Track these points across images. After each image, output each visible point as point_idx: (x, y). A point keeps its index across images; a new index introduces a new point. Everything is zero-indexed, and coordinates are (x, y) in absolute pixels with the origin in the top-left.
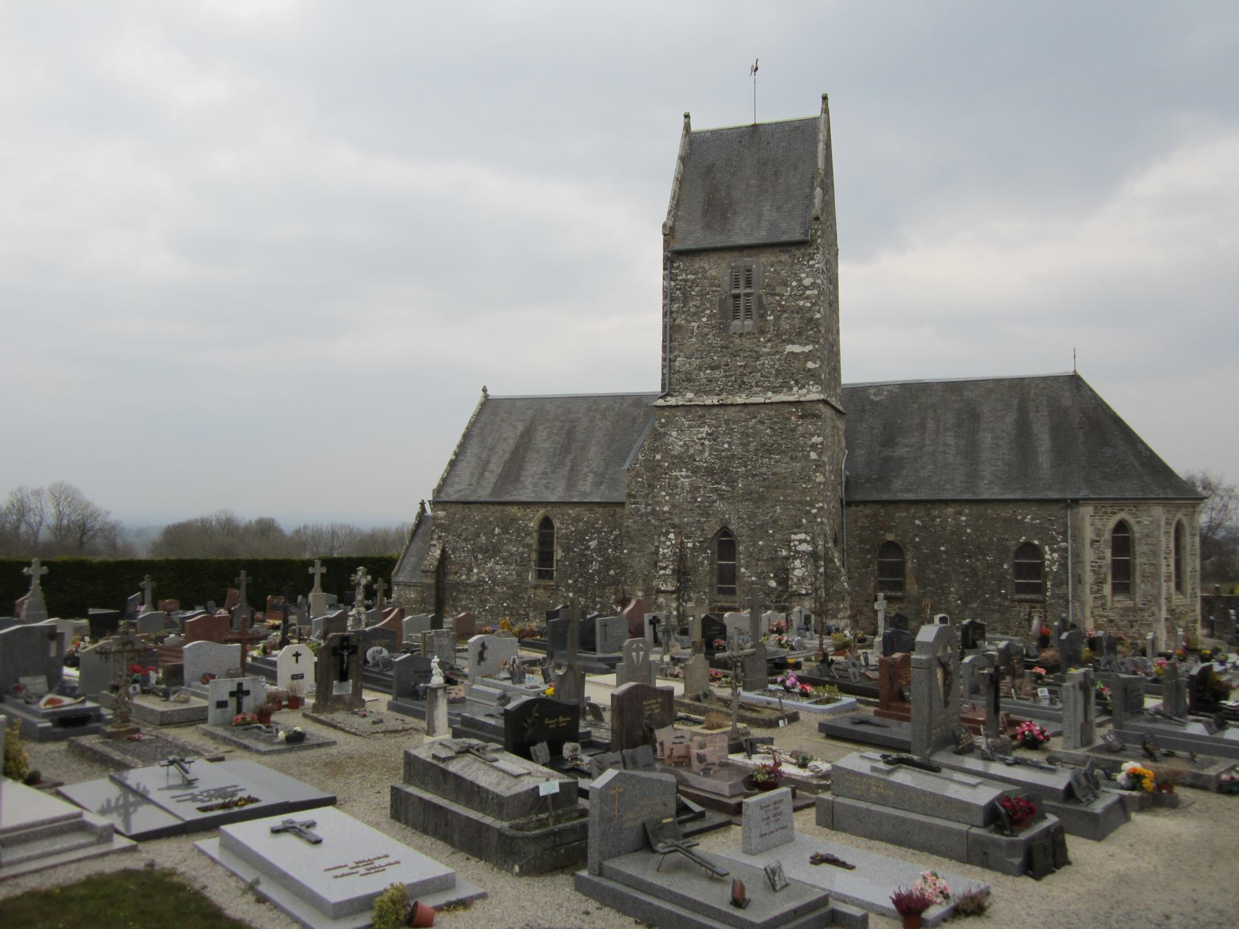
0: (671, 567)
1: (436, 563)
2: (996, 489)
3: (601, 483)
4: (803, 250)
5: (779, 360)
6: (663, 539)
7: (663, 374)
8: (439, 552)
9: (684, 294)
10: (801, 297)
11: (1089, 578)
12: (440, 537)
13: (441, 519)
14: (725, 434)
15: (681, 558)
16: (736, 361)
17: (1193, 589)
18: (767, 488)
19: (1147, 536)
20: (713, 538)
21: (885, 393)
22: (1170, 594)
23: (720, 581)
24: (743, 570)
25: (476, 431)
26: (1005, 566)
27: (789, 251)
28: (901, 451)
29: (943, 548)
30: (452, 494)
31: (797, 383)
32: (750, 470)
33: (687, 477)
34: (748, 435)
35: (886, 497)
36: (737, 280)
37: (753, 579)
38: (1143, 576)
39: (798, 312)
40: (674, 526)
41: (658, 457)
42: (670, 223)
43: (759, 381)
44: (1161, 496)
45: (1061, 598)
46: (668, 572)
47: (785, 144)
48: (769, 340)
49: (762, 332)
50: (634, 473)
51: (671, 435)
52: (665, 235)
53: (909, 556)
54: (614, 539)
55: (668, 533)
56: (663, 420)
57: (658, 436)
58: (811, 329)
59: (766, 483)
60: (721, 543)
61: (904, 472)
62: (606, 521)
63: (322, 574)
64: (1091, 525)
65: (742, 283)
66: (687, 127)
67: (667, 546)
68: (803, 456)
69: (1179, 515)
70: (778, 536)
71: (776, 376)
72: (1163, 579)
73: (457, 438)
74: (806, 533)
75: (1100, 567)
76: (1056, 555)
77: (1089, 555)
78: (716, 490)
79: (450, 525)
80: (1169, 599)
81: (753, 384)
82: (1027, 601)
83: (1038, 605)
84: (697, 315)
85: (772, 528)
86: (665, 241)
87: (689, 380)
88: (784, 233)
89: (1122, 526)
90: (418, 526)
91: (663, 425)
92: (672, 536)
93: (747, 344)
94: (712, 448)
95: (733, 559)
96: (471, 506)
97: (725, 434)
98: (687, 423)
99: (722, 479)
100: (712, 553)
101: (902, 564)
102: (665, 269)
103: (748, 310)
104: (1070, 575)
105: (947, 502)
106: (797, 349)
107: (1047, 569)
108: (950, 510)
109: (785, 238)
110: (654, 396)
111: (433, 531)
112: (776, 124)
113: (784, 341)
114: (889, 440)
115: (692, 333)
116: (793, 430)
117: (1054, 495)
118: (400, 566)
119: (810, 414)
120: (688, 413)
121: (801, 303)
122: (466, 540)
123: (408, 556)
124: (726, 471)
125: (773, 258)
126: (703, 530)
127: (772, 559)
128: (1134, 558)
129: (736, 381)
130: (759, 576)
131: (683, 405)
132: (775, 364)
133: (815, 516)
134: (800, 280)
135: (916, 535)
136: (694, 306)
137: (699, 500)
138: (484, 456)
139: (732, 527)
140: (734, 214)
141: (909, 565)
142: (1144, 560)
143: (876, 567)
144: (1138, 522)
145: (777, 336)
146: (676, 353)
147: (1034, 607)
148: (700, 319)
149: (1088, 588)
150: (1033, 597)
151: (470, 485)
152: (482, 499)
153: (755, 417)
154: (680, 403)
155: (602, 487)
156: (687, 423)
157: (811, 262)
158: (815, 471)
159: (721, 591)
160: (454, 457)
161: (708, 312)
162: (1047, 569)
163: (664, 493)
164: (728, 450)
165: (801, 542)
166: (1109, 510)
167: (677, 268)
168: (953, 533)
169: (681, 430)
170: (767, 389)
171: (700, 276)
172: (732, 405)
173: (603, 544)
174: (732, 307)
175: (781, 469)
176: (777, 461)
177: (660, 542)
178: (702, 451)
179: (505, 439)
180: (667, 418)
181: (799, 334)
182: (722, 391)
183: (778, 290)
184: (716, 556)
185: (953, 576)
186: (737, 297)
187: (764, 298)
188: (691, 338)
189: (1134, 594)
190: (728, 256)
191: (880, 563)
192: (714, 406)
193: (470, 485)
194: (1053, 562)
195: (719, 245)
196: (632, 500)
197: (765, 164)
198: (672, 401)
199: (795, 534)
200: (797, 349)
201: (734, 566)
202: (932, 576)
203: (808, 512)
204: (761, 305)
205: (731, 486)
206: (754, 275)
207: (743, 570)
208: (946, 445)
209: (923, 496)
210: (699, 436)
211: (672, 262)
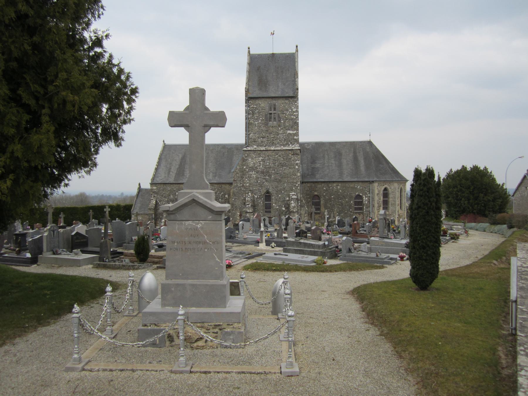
0: (250, 204)
1: (154, 206)
2: (349, 178)
3: (215, 176)
4: (293, 99)
5: (285, 135)
6: (247, 195)
7: (246, 139)
8: (155, 202)
9: (253, 112)
10: (292, 115)
11: (376, 205)
12: (154, 196)
13: (155, 190)
14: (267, 160)
15: (253, 201)
16: (271, 135)
17: (404, 208)
18: (282, 178)
19: (393, 192)
20: (263, 195)
21: (310, 146)
22: (399, 210)
23: (266, 209)
24: (274, 205)
25: (163, 157)
26: (352, 202)
27: (288, 99)
28: (318, 165)
29: (332, 197)
30: (158, 180)
31: (291, 143)
32: (276, 172)
33: (255, 174)
34: (275, 160)
35: (315, 180)
36: (271, 108)
37: (277, 207)
38: (392, 204)
39: (291, 120)
40: (250, 191)
41: (245, 167)
42: (247, 88)
43: (279, 142)
44: (397, 180)
45: (368, 212)
46: (250, 206)
47: (284, 61)
48: (282, 129)
49: (279, 126)
50: (236, 173)
51: (249, 160)
52: (246, 91)
53: (322, 199)
54: (222, 196)
55: (248, 193)
56: (246, 155)
57: (244, 160)
58: (296, 126)
59: (281, 176)
60: (266, 196)
61: (320, 172)
62: (218, 190)
63: (109, 211)
64: (377, 189)
65: (273, 109)
66: (249, 52)
67: (249, 197)
68: (293, 167)
69: (401, 186)
70: (285, 193)
71: (284, 141)
72: (397, 205)
73: (156, 160)
74: (295, 192)
75: (379, 202)
76: (367, 198)
77: (376, 198)
78: (265, 179)
79: (158, 192)
80: (398, 211)
81: (277, 143)
82: (358, 213)
83: (361, 214)
84: (257, 120)
85: (283, 191)
86: (246, 93)
87: (255, 142)
88: (287, 93)
89: (386, 189)
90: (139, 192)
91: (246, 157)
92: (250, 194)
93: (275, 130)
94: (263, 165)
95: (270, 201)
96: (166, 185)
97: (267, 160)
98: (254, 156)
99: (267, 175)
100: (263, 199)
101: (320, 202)
102: (246, 103)
103: (275, 118)
104: (371, 204)
105: (334, 182)
106: (291, 132)
107: (364, 203)
108: (335, 184)
109: (287, 95)
110: (241, 146)
111: (152, 194)
112: (280, 54)
113: (287, 129)
114: (313, 162)
115: (256, 126)
116: (290, 159)
117: (367, 180)
118: (134, 208)
119: (295, 154)
120: (255, 152)
121: (292, 117)
122: (165, 197)
123: (136, 203)
124: (268, 172)
125: (283, 101)
126: (261, 192)
127: (283, 201)
128: (389, 199)
129: (271, 142)
130: (279, 206)
131: (253, 150)
132: (284, 137)
133: (297, 187)
134: (292, 109)
135: (324, 193)
136: (256, 116)
137: (259, 182)
138: (168, 166)
139: (270, 191)
140: (269, 85)
141: (322, 202)
142: (392, 200)
143: (311, 203)
144: (390, 188)
145: (284, 127)
146: (250, 132)
147: (360, 215)
148: (258, 120)
149: (376, 208)
150: (360, 211)
151: (165, 177)
152: (171, 182)
153: (277, 154)
154: (252, 149)
155: (217, 177)
156: (254, 156)
157: (296, 104)
158: (297, 172)
159: (266, 212)
160: (157, 167)
161: (261, 118)
162: (364, 203)
163: (247, 180)
164: (269, 165)
165: (293, 195)
166: (382, 184)
167: (250, 103)
168: (335, 192)
169: (252, 158)
170: (281, 145)
171: (258, 106)
172: (270, 150)
173: (218, 197)
174: (269, 117)
175: (286, 172)
176: (285, 169)
177: (246, 196)
178: (260, 166)
179: (175, 160)
180: (247, 154)
181: (292, 127)
182: (266, 145)
183: (285, 112)
184: (264, 200)
185: (336, 205)
186: (271, 114)
187: (280, 115)
188: (255, 127)
189: (389, 210)
190: (268, 100)
191: (312, 202)
192: (264, 150)
193: (165, 177)
194: (366, 200)
195: (265, 96)
196: (235, 182)
197: (278, 68)
198: (249, 149)
199: (291, 193)
200: (291, 132)
201: (270, 203)
202: (329, 206)
203: (295, 186)
204: (279, 117)
205: (270, 177)
206: (277, 107)
207: (274, 205)
208: (332, 163)
209: (326, 180)
210: (259, 160)
211: (249, 101)
